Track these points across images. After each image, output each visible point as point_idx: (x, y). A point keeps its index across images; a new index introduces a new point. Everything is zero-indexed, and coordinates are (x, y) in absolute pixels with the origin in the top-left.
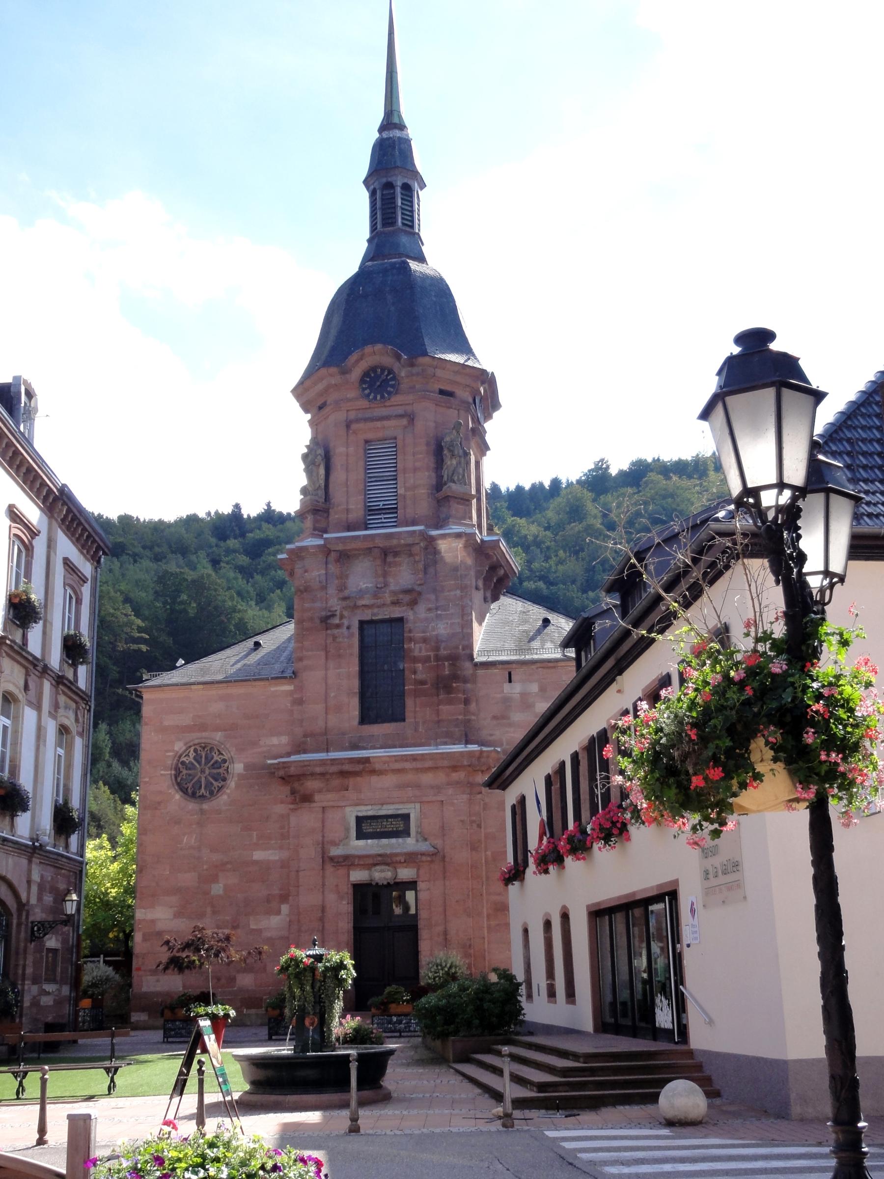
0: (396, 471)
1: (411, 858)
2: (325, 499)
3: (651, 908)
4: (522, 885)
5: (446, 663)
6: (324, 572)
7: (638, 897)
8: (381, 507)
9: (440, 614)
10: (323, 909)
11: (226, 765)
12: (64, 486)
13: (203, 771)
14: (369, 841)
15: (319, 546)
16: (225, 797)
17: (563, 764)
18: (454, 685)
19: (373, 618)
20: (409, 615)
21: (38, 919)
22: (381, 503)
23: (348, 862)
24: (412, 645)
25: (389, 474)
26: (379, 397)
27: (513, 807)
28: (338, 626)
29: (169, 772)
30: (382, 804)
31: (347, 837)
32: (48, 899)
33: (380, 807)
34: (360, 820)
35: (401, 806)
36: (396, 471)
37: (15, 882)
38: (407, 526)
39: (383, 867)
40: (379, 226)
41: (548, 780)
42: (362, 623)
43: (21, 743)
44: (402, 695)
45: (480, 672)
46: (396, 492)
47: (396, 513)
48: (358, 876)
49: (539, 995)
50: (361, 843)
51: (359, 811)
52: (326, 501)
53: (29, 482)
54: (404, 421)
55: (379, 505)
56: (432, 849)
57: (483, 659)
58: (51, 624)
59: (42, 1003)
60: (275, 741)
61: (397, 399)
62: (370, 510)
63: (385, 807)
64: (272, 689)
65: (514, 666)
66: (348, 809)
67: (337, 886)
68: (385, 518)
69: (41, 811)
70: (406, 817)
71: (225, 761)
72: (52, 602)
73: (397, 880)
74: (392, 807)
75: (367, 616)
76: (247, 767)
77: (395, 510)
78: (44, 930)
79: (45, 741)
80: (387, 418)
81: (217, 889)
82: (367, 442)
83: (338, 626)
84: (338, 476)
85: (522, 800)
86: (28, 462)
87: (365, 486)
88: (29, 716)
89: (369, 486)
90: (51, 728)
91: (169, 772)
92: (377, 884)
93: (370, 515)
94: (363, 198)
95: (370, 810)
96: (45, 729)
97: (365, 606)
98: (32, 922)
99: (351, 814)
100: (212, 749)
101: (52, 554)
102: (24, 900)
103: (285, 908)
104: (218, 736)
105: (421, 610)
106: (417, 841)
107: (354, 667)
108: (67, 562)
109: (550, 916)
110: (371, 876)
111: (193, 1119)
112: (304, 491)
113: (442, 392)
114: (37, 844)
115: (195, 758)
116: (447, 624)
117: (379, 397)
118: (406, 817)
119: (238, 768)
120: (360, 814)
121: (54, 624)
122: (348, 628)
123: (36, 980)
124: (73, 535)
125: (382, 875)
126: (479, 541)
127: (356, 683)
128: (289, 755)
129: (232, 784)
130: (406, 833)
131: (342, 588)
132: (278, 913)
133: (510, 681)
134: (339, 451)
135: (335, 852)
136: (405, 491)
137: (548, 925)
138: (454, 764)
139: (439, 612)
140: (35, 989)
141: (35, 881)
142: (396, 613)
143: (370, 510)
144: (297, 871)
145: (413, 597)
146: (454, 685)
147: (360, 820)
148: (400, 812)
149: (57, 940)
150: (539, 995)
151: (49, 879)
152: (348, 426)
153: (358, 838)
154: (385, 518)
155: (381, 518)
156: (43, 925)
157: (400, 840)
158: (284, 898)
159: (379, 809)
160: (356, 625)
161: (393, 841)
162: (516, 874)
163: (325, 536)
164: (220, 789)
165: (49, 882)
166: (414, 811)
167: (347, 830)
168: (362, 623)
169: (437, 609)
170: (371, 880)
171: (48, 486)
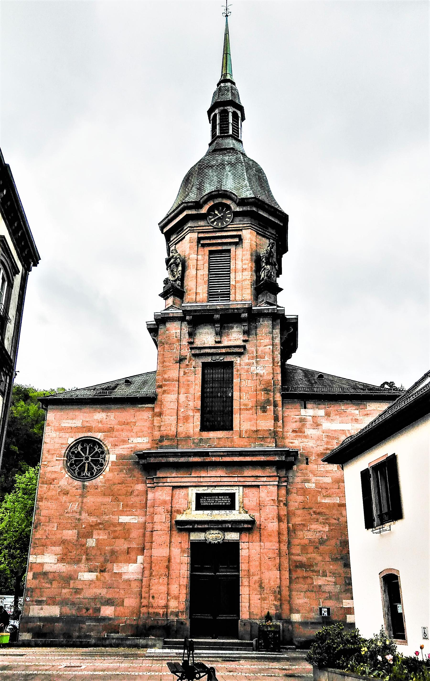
13: (87, 459)
16: (101, 477)
22: (219, 291)
67: (180, 543)
70: (232, 496)
81: (91, 543)
103: (140, 558)
104: (99, 436)
119: (112, 457)
132: (135, 562)
158: (142, 550)
167: (189, 503)
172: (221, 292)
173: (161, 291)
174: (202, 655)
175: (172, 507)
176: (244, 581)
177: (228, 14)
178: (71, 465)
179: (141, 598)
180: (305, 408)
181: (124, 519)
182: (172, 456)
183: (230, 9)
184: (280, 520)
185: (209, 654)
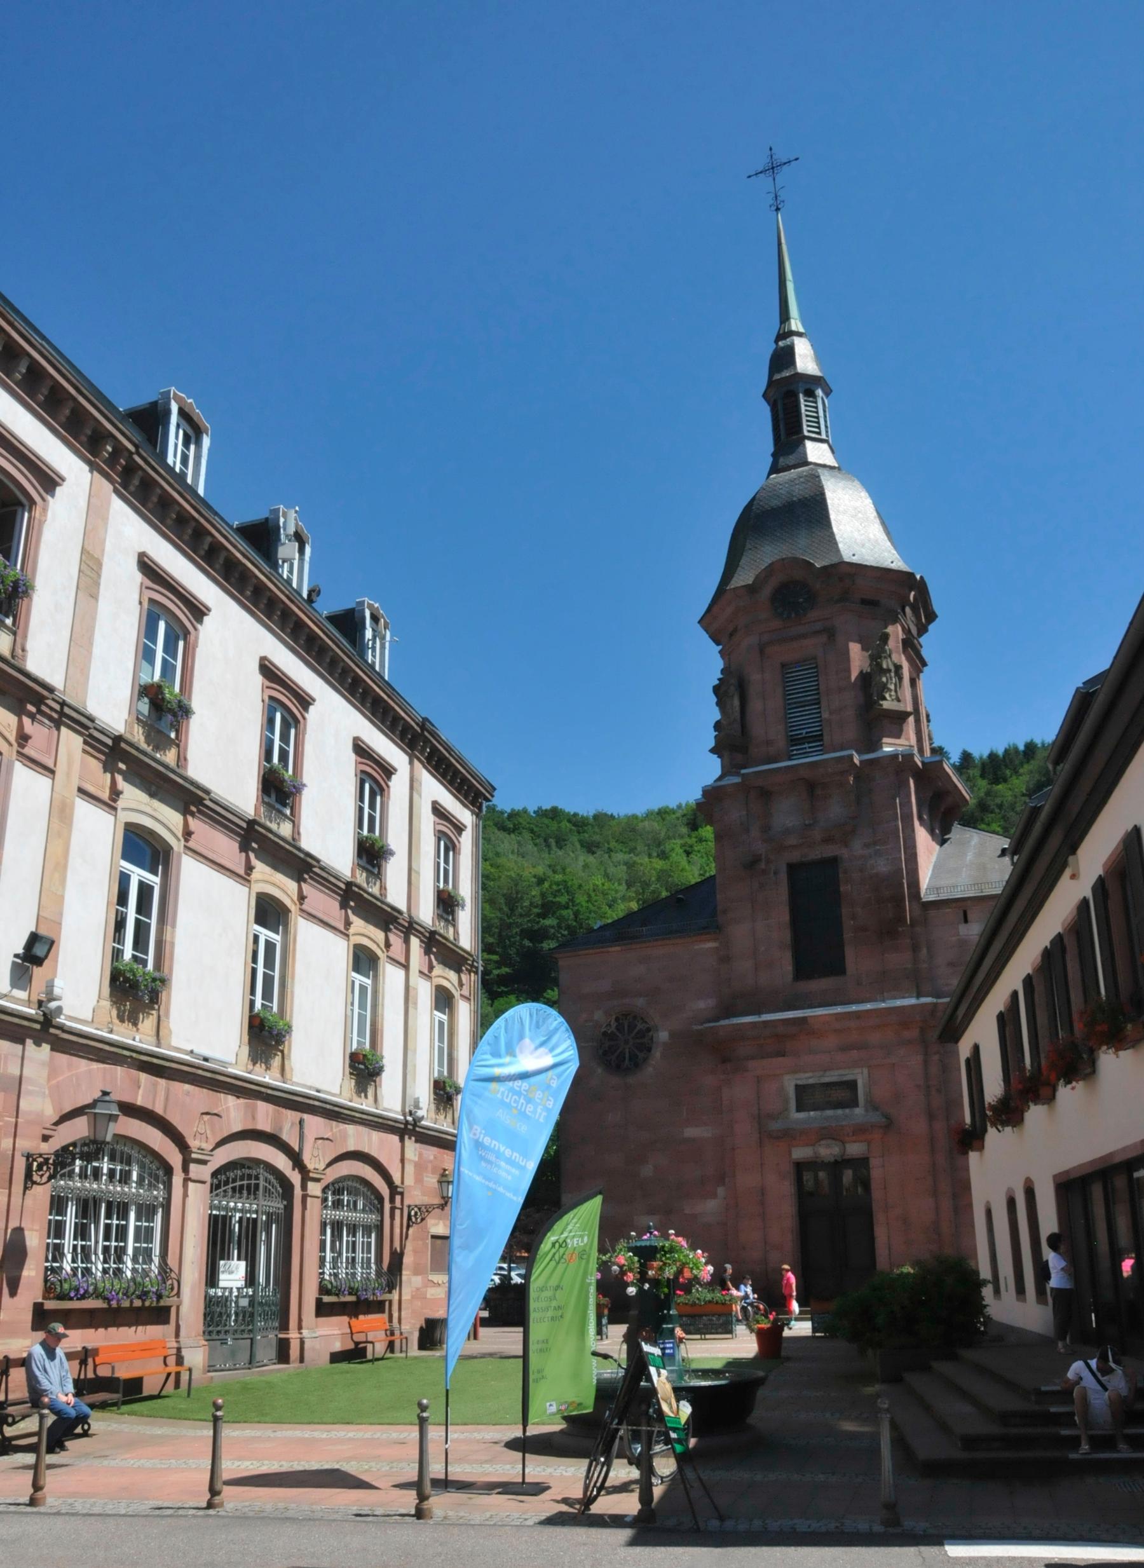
0: (818, 694)
1: (860, 1131)
2: (742, 731)
3: (1136, 1175)
4: (981, 1155)
5: (889, 905)
6: (745, 813)
7: (1117, 1160)
8: (804, 735)
9: (879, 850)
10: (763, 1191)
11: (651, 1034)
12: (425, 720)
13: (626, 1042)
14: (812, 1113)
15: (737, 784)
16: (650, 1069)
17: (1015, 994)
18: (900, 929)
19: (803, 860)
20: (844, 853)
21: (418, 1203)
22: (804, 731)
23: (789, 1136)
24: (849, 886)
25: (809, 698)
26: (793, 615)
27: (968, 1061)
28: (764, 872)
29: (591, 1044)
30: (825, 1071)
31: (786, 1109)
32: (432, 1180)
33: (821, 1073)
34: (800, 1090)
35: (846, 1071)
36: (818, 694)
37: (383, 1160)
38: (835, 751)
39: (830, 1141)
40: (783, 437)
41: (1001, 1017)
42: (791, 868)
43: (383, 1005)
44: (840, 946)
45: (932, 913)
46: (821, 717)
47: (822, 740)
48: (801, 1153)
49: (1007, 1291)
50: (802, 1115)
51: (799, 1079)
52: (743, 735)
53: (379, 715)
54: (823, 638)
55: (801, 734)
56: (884, 1120)
57: (932, 898)
58: (418, 873)
59: (428, 1296)
60: (701, 1005)
61: (813, 614)
62: (792, 740)
63: (828, 1073)
64: (696, 947)
65: (969, 902)
66: (786, 1078)
67: (778, 1164)
68: (810, 747)
69: (415, 1082)
70: (852, 1085)
71: (649, 1030)
72: (419, 852)
73: (846, 1157)
74: (836, 1073)
75: (795, 856)
76: (672, 1035)
77: (819, 738)
78: (421, 1214)
79: (416, 1004)
80: (804, 636)
81: (647, 1171)
82: (783, 666)
83: (764, 872)
84: (756, 706)
85: (976, 1049)
86: (374, 691)
87: (786, 714)
88: (392, 977)
89: (790, 713)
90: (424, 992)
91: (591, 1044)
92: (823, 1162)
93: (792, 746)
94: (765, 411)
95: (811, 1078)
96: (416, 989)
97: (794, 847)
98: (409, 1206)
99: (790, 1084)
100: (635, 1017)
101: (415, 796)
102: (397, 1180)
103: (721, 1191)
104: (640, 1002)
105: (857, 847)
106: (867, 1111)
107: (783, 915)
108: (438, 811)
109: (1014, 1192)
110: (815, 1153)
111: (31, 1469)
112: (718, 726)
113: (864, 602)
114: (410, 1119)
115: (617, 1028)
116: (888, 859)
117: (793, 615)
118: (852, 1085)
119: (663, 1036)
120: (800, 1082)
121: (421, 874)
122: (775, 873)
123: (417, 1271)
124: (444, 776)
125: (828, 1151)
126: (920, 764)
127: (787, 935)
128: (717, 1019)
129: (657, 1053)
130: (854, 1103)
131: (766, 828)
132: (714, 1196)
133: (966, 921)
134: (755, 677)
135: (775, 1126)
136: (831, 713)
137: (1011, 1203)
138: (903, 1017)
139: (878, 847)
140: (417, 1281)
141: (410, 1160)
142: (829, 851)
143: (792, 740)
144: (733, 1149)
145: (844, 833)
146: (900, 929)
147: (800, 1090)
148: (845, 1079)
149: (445, 1225)
150: (1007, 1291)
151: (432, 1158)
152: (762, 652)
153: (799, 1110)
154: (810, 747)
155: (805, 748)
156: (419, 1209)
157: (847, 1111)
158: (721, 1179)
159: (823, 1076)
160: (783, 869)
161: (840, 1112)
162: (971, 1139)
163: (743, 771)
164: (645, 1060)
165: (431, 1162)
166: (861, 1077)
167: (786, 1101)
168: (791, 868)
169: (875, 843)
170: (817, 1158)
171: (403, 719)
172: (807, 733)
173: (712, 744)
174: (453, 753)
175: (759, 1109)
176: (879, 1218)
177: (780, 206)
178: (605, 1053)
179: (719, 1315)
180: (966, 921)
181: (691, 1132)
182: (791, 664)
183: (782, 195)
184: (931, 1116)
185: (324, 625)
